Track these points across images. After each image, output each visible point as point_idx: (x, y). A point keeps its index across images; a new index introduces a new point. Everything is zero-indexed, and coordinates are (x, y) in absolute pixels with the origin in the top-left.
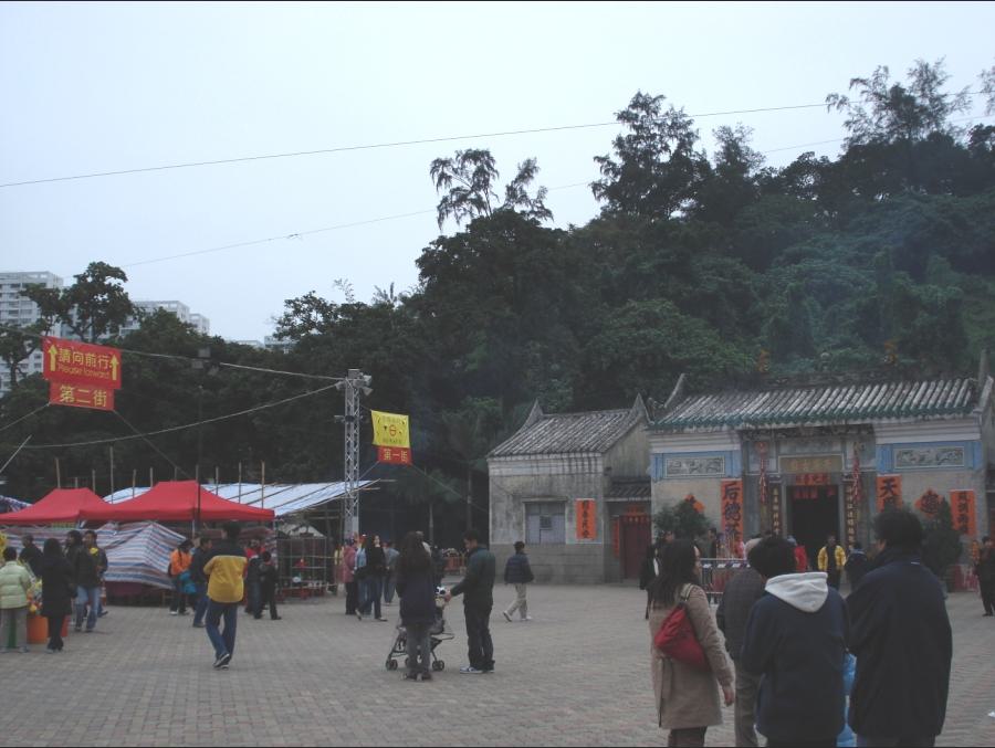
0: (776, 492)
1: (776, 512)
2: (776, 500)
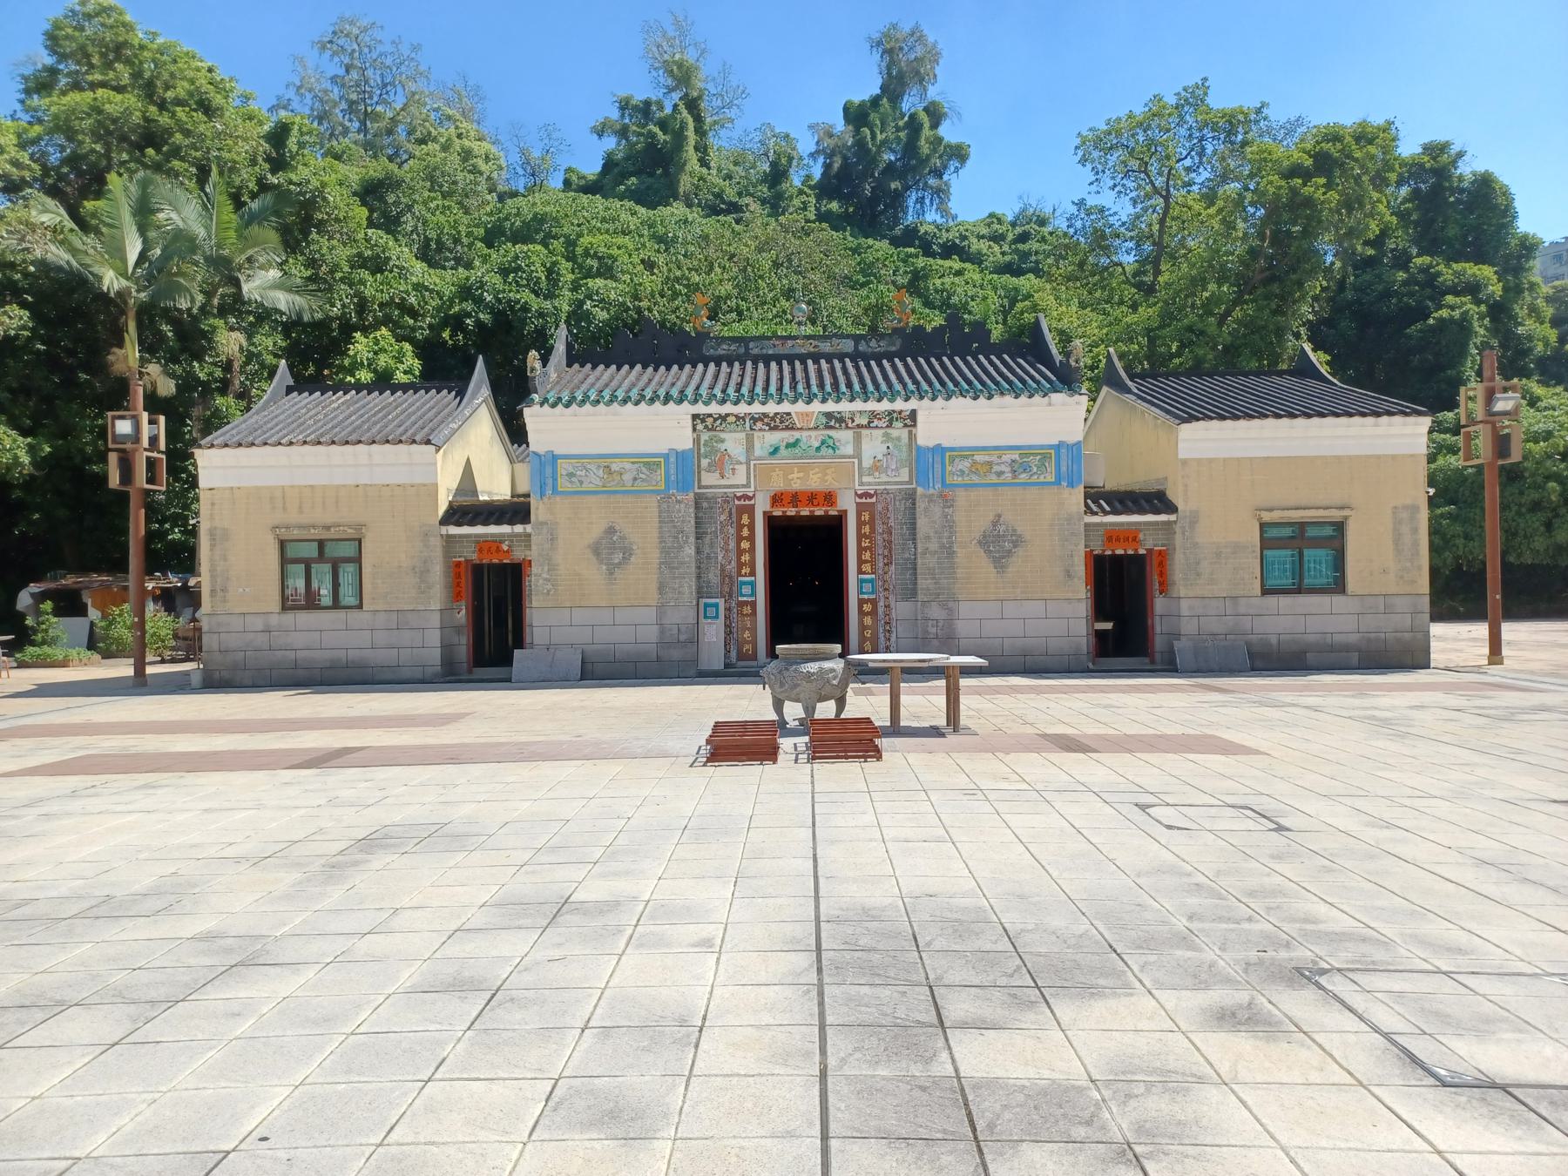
0: (745, 520)
1: (865, 523)
2: (745, 532)
